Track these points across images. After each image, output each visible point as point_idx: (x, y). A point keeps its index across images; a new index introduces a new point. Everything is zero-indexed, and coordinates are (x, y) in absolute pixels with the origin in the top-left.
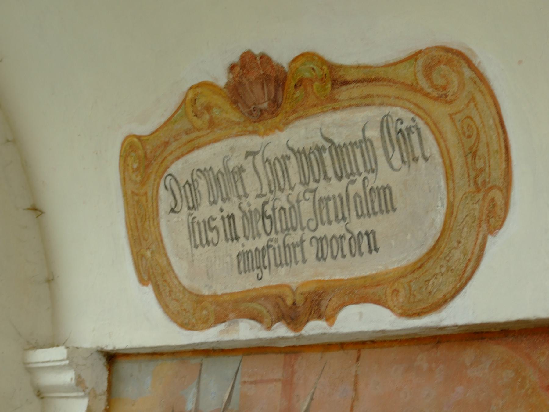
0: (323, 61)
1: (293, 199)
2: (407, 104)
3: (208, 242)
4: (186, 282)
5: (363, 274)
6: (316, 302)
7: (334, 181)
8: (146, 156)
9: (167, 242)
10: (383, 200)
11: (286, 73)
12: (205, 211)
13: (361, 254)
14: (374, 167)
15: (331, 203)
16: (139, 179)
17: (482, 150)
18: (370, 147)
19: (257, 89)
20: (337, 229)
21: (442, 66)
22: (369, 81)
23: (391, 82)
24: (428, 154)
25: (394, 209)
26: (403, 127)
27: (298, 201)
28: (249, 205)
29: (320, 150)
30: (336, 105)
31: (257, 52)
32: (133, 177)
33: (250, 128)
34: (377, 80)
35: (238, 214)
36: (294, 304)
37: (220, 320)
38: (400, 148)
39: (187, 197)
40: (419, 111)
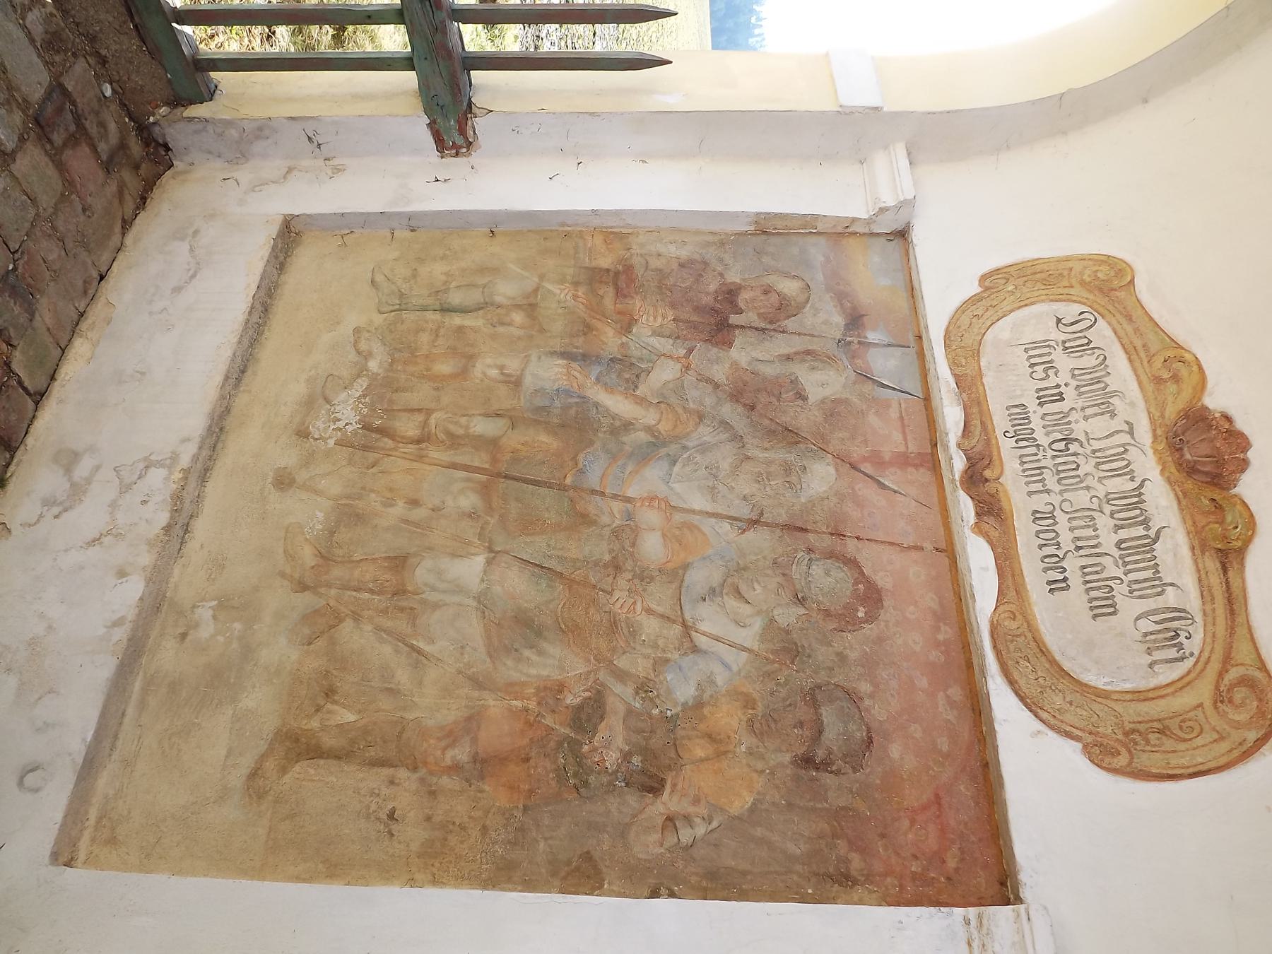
0: (1248, 541)
1: (1090, 481)
2: (1208, 649)
3: (1032, 365)
4: (989, 336)
5: (1025, 573)
6: (991, 510)
7: (1114, 538)
8: (1112, 290)
9: (1026, 311)
10: (1103, 607)
11: (1228, 489)
12: (1065, 363)
13: (1045, 570)
14: (1136, 593)
15: (1090, 532)
16: (1086, 278)
17: (1169, 744)
18: (1155, 590)
19: (1204, 449)
20: (1066, 539)
21: (1255, 703)
22: (1230, 600)
23: (1231, 630)
24: (1156, 668)
25: (1094, 617)
26: (1182, 639)
27: (1088, 488)
28: (1077, 422)
29: (1145, 523)
30: (1197, 551)
31: (1250, 454)
32: (1088, 272)
33: (1159, 432)
34: (1232, 612)
35: (1064, 406)
36: (987, 480)
37: (959, 379)
38: (1159, 632)
39: (1074, 339)
40: (1202, 664)
